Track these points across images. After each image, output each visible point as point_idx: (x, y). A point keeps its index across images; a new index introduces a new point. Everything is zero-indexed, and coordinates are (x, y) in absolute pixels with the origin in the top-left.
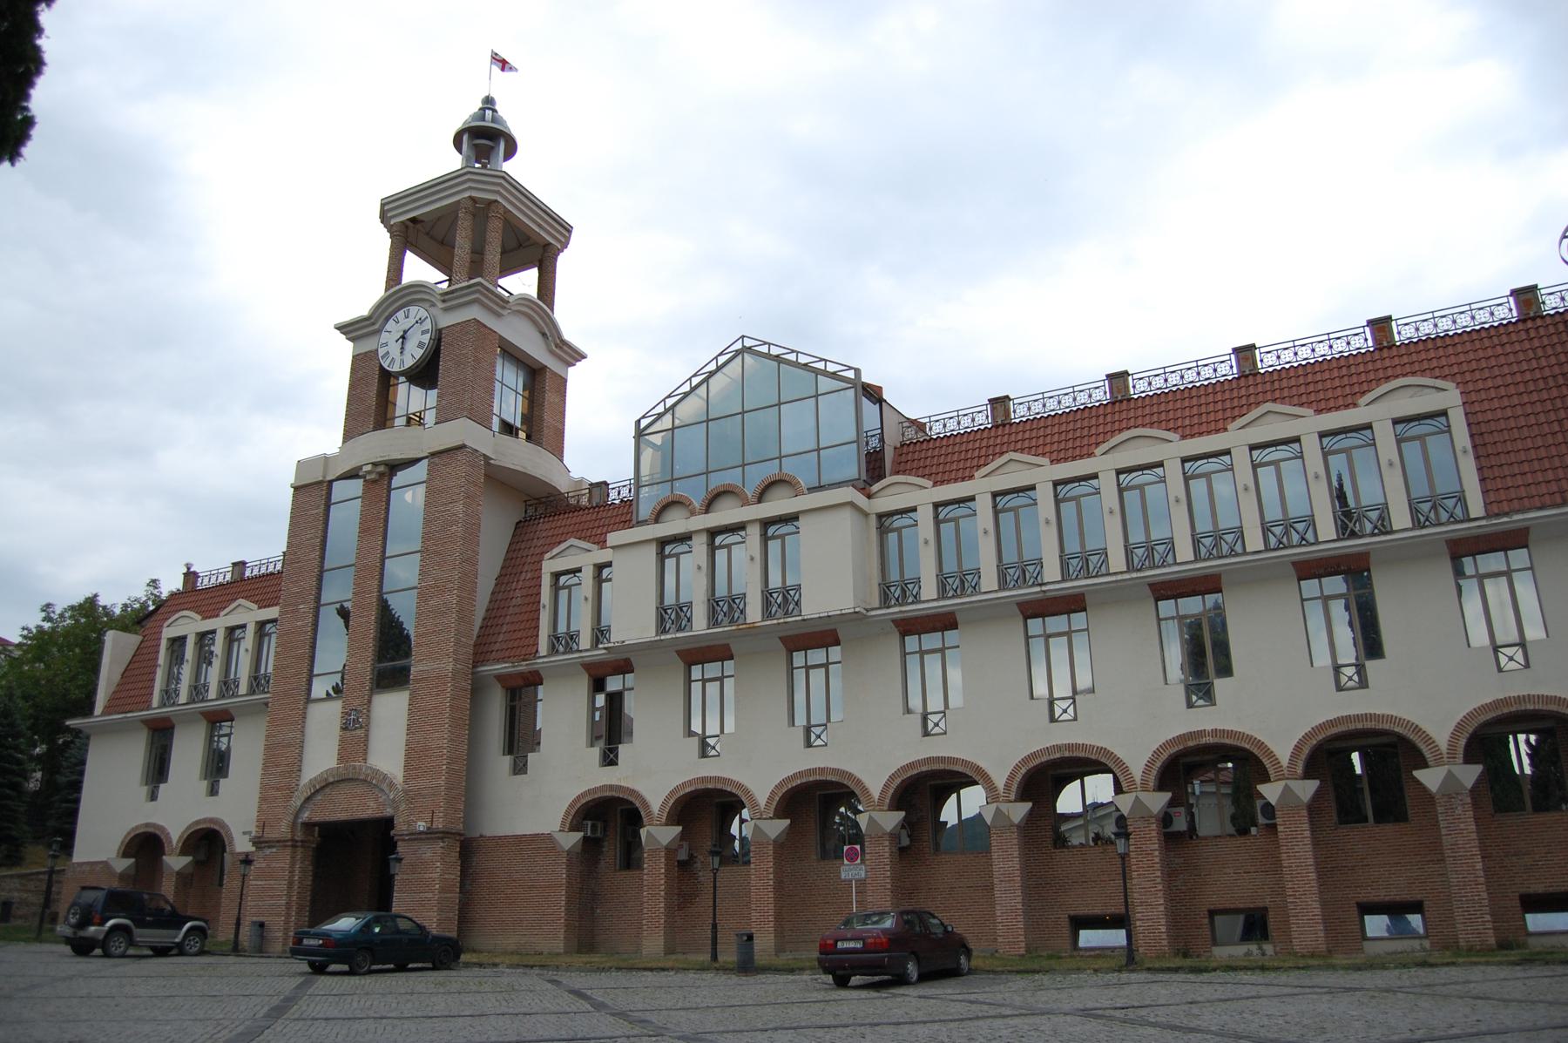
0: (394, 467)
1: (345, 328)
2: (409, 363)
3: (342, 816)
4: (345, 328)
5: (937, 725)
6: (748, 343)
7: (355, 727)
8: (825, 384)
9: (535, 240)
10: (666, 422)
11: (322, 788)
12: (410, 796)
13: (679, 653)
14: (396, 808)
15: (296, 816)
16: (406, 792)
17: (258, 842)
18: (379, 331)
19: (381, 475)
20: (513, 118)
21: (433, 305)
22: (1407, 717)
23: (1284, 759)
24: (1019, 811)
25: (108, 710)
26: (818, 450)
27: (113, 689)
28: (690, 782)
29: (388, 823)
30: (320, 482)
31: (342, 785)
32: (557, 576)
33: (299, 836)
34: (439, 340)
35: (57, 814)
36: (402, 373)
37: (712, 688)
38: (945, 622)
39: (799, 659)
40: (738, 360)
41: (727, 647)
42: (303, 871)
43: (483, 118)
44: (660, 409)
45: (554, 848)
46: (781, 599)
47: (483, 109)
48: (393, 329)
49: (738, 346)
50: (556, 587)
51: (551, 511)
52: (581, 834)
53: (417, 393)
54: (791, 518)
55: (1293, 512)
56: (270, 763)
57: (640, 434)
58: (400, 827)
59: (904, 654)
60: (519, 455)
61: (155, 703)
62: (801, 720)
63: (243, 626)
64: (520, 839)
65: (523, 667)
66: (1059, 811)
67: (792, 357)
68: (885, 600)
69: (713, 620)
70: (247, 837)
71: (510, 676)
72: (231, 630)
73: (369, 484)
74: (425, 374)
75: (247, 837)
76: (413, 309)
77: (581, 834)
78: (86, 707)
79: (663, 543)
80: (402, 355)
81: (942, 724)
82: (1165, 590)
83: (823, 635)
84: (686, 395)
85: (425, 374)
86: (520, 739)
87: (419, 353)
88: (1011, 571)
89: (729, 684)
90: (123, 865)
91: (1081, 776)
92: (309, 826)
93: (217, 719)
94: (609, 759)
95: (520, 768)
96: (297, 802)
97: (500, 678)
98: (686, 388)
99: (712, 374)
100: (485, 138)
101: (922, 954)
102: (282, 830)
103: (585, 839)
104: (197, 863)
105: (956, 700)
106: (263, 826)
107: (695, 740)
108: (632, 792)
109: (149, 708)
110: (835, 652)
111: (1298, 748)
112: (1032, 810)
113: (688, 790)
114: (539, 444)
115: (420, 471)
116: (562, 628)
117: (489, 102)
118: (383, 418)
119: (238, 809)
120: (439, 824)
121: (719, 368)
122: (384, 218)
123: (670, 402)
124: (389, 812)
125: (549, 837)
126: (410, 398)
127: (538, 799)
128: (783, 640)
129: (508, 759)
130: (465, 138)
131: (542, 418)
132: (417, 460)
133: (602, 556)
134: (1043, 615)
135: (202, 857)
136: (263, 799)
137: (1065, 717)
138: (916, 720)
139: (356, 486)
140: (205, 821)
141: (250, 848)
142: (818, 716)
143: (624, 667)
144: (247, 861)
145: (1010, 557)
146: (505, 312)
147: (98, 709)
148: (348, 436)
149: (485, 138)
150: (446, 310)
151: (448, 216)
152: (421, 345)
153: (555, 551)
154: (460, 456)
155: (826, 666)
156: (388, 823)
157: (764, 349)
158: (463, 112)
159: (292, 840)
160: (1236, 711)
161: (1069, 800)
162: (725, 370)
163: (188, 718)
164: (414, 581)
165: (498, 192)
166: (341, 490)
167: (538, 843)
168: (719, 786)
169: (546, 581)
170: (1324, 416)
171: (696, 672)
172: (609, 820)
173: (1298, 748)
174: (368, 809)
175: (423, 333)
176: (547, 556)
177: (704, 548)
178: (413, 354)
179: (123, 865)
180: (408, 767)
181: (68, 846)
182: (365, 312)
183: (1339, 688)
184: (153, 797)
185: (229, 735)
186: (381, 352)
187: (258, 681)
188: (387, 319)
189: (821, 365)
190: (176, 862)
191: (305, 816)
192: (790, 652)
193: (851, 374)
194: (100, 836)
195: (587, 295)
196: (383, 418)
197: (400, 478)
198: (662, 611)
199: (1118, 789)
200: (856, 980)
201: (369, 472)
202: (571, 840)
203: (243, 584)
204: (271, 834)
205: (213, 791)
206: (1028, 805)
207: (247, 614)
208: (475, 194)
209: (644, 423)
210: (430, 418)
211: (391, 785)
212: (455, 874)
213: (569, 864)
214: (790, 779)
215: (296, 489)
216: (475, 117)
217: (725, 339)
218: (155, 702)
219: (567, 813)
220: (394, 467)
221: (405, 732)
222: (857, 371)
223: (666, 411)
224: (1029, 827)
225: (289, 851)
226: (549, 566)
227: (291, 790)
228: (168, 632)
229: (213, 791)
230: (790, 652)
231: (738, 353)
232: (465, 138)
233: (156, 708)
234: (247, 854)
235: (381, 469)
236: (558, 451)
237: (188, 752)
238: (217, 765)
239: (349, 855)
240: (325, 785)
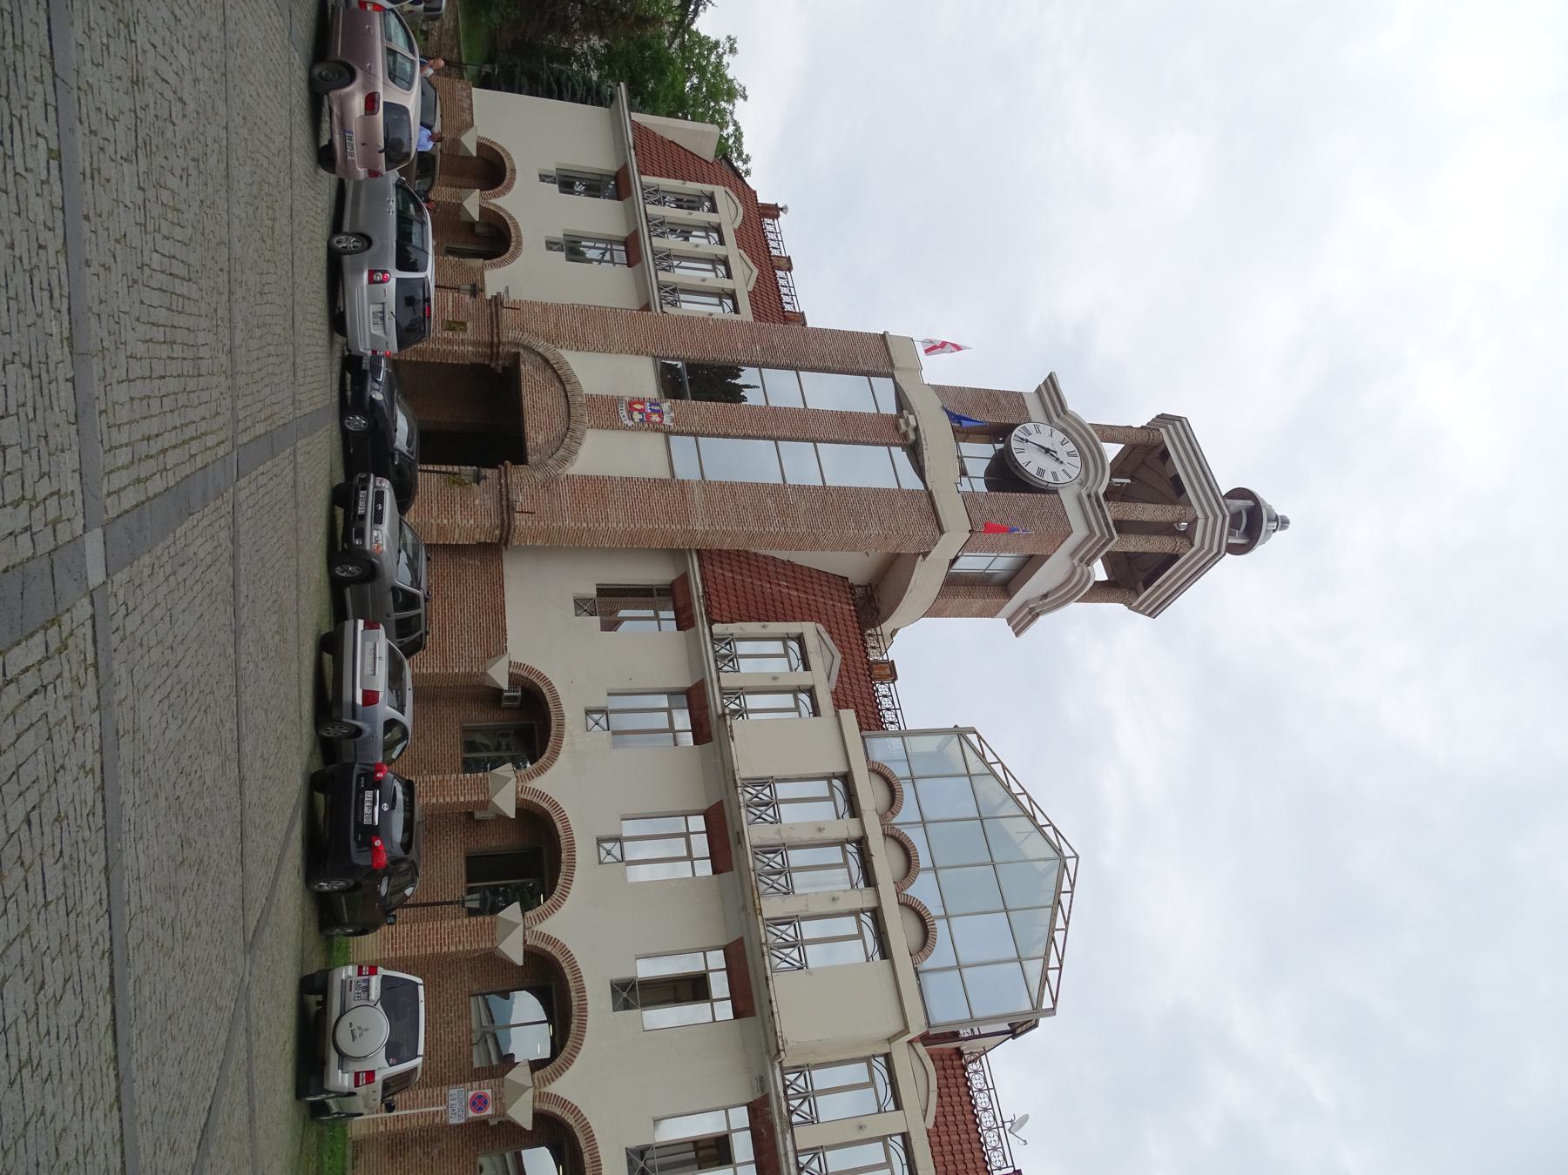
0: (915, 452)
2: (1021, 459)
3: (527, 402)
5: (609, 853)
6: (1071, 863)
8: (1034, 968)
10: (976, 766)
11: (559, 377)
12: (550, 484)
13: (721, 802)
14: (537, 467)
15: (526, 347)
16: (555, 480)
17: (497, 301)
18: (1050, 421)
19: (905, 436)
20: (1272, 546)
21: (1082, 484)
22: (589, 1001)
24: (522, 1113)
25: (637, 127)
26: (959, 967)
27: (658, 132)
28: (568, 829)
29: (520, 458)
30: (892, 366)
31: (563, 400)
32: (800, 639)
33: (503, 350)
35: (526, 68)
36: (1008, 446)
40: (1052, 854)
41: (709, 739)
42: (463, 356)
43: (1269, 520)
44: (990, 758)
45: (490, 656)
47: (1276, 519)
48: (1053, 439)
49: (1067, 852)
52: (506, 687)
54: (885, 951)
55: (797, 878)
56: (587, 314)
57: (960, 733)
58: (517, 474)
60: (926, 579)
61: (645, 179)
62: (628, 829)
63: (729, 275)
64: (499, 611)
65: (698, 608)
66: (525, 1153)
67: (1060, 923)
70: (502, 291)
71: (687, 591)
72: (725, 262)
73: (894, 422)
74: (1005, 475)
75: (502, 291)
76: (1077, 461)
77: (506, 687)
78: (644, 100)
79: (847, 779)
81: (609, 859)
84: (1008, 788)
85: (1005, 475)
87: (1032, 469)
88: (767, 791)
89: (683, 870)
90: (469, 143)
91: (550, 1020)
93: (631, 249)
95: (582, 606)
96: (542, 346)
97: (684, 578)
98: (1015, 789)
99: (1033, 819)
101: (343, 873)
103: (501, 691)
104: (471, 225)
105: (639, 874)
108: (556, 752)
109: (641, 173)
110: (705, 868)
111: (554, 942)
112: (513, 965)
113: (559, 826)
114: (941, 594)
115: (911, 481)
116: (683, 297)
117: (1283, 523)
118: (964, 428)
119: (528, 277)
120: (520, 520)
121: (1039, 828)
122: (1163, 419)
123: (998, 769)
124: (532, 459)
126: (979, 454)
127: (543, 629)
128: (740, 941)
129: (593, 592)
130: (1250, 503)
131: (967, 592)
132: (920, 471)
133: (825, 700)
134: (709, 831)
135: (478, 229)
136: (545, 308)
137: (603, 853)
138: (602, 701)
139: (889, 407)
140: (519, 237)
141: (490, 293)
142: (618, 722)
143: (701, 732)
144: (476, 291)
146: (1075, 561)
147: (638, 117)
148: (940, 390)
150: (1079, 498)
151: (1175, 490)
152: (1041, 471)
153: (826, 636)
154: (930, 527)
155: (690, 857)
156: (520, 458)
157: (1066, 886)
158: (1273, 500)
159: (499, 343)
161: (526, 1006)
162: (1038, 835)
163: (631, 216)
164: (789, 481)
165: (1207, 518)
166: (884, 386)
167: (496, 641)
168: (564, 868)
170: (893, 887)
172: (526, 722)
173: (555, 942)
174: (536, 435)
175: (1054, 474)
176: (820, 627)
177: (843, 835)
178: (1029, 460)
179: (469, 143)
180: (586, 479)
181: (486, 83)
182: (1070, 407)
183: (600, 841)
184: (544, 178)
185: (612, 261)
186: (1030, 426)
187: (673, 292)
188: (1063, 431)
189: (1053, 962)
190: (473, 204)
191: (524, 354)
193: (1047, 1003)
194: (505, 119)
195: (1097, 640)
196: (964, 428)
197: (900, 455)
199: (536, 1065)
200: (320, 798)
201: (907, 423)
202: (499, 675)
204: (506, 315)
205: (551, 245)
206: (519, 961)
207: (744, 277)
208: (1200, 522)
209: (973, 738)
210: (966, 486)
211: (565, 460)
212: (458, 538)
213: (470, 675)
214: (573, 964)
215: (883, 336)
216: (1270, 510)
217: (1074, 836)
218: (648, 179)
219: (531, 670)
220: (915, 452)
221: (625, 475)
222: (1052, 1011)
223: (988, 765)
224: (492, 961)
225: (487, 338)
226: (809, 629)
227: (554, 340)
228: (719, 192)
231: (1059, 851)
232: (1250, 503)
233: (642, 181)
234: (482, 290)
235: (912, 436)
236: (934, 612)
237: (598, 217)
239: (480, 412)
240: (560, 378)
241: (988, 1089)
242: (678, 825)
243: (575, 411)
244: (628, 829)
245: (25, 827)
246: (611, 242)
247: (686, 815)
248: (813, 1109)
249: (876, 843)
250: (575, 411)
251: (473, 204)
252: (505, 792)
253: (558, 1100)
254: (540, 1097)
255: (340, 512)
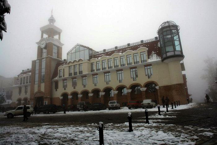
1: (37, 43)
4: (37, 43)
7: (39, 86)
8: (85, 49)
9: (58, 32)
10: (70, 53)
23: (69, 94)
34: (46, 46)
37: (120, 74)
38: (121, 70)
39: (106, 74)
46: (81, 72)
50: (60, 71)
51: (60, 63)
53: (45, 50)
59: (117, 74)
68: (69, 76)
69: (74, 75)
74: (45, 48)
80: (43, 46)
82: (131, 68)
83: (85, 76)
86: (57, 87)
90: (61, 98)
92: (35, 98)
94: (65, 89)
95: (56, 90)
100: (52, 20)
102: (33, 98)
106: (30, 98)
107: (132, 79)
124: (43, 96)
125: (15, 102)
138: (106, 83)
143: (66, 80)
145: (116, 65)
149: (52, 20)
155: (86, 79)
160: (138, 81)
169: (58, 71)
171: (106, 74)
182: (39, 41)
183: (134, 80)
192: (105, 74)
197: (43, 60)
198: (69, 74)
203: (28, 71)
229: (20, 95)
230: (105, 74)
238: (26, 92)
240: (36, 93)
241: (147, 40)
242: (146, 70)
243: (39, 91)
244: (106, 81)
245: (120, 136)
246: (63, 82)
247: (131, 71)
248: (145, 60)
249: (79, 63)
250: (39, 91)
251: (70, 97)
252: (91, 95)
253: (144, 85)
254: (115, 91)
255: (131, 108)
